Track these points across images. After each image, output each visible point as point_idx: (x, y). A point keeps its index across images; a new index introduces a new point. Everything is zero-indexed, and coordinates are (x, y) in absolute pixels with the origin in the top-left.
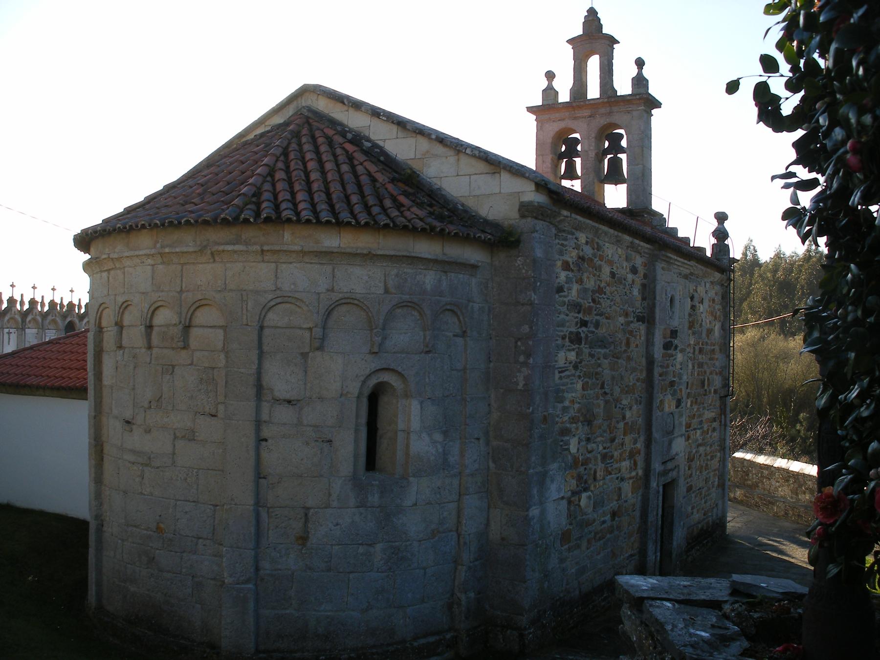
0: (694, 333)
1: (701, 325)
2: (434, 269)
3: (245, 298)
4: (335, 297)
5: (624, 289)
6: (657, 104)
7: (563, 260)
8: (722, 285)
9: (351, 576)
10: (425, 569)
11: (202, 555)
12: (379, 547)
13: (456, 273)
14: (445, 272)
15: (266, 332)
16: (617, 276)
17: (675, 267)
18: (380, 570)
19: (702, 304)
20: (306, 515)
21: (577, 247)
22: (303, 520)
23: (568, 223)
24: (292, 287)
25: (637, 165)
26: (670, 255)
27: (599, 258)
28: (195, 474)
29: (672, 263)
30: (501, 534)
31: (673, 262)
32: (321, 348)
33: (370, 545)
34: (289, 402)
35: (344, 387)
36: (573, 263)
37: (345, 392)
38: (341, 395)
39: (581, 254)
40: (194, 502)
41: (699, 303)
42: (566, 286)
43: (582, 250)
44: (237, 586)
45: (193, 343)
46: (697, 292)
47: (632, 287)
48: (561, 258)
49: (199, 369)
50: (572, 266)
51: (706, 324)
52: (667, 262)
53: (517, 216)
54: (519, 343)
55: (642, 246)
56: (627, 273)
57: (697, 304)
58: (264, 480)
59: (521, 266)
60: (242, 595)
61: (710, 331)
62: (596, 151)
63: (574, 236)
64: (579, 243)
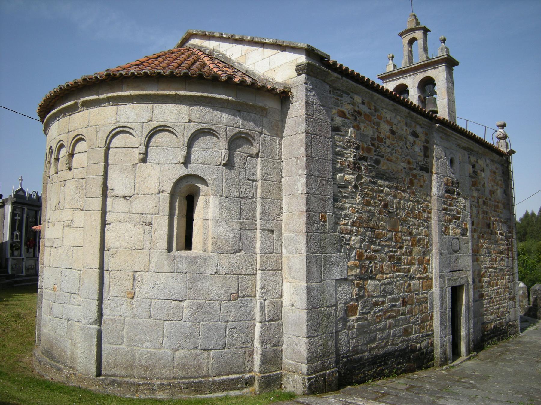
0: (477, 190)
1: (484, 186)
2: (229, 107)
3: (98, 130)
4: (154, 125)
5: (406, 144)
6: (429, 31)
7: (338, 109)
8: (502, 165)
9: (166, 323)
10: (226, 322)
11: (73, 305)
12: (185, 304)
13: (248, 112)
14: (239, 111)
15: (111, 151)
16: (396, 133)
17: (453, 139)
18: (187, 320)
19: (484, 172)
20: (134, 276)
21: (353, 104)
22: (132, 280)
23: (341, 84)
24: (126, 120)
25: (444, 99)
26: (446, 128)
27: (377, 117)
28: (71, 250)
29: (450, 136)
30: (290, 301)
31: (450, 134)
32: (144, 160)
33: (180, 301)
34: (124, 197)
35: (161, 187)
36: (349, 113)
37: (161, 190)
38: (159, 192)
39: (357, 109)
40: (70, 269)
41: (481, 171)
42: (343, 128)
43: (358, 107)
44: (88, 326)
45: (74, 164)
46: (477, 162)
47: (413, 145)
48: (337, 108)
49: (76, 181)
50: (347, 115)
51: (489, 185)
52: (445, 134)
53: (295, 74)
54: (299, 161)
55: (419, 119)
56: (408, 135)
57: (479, 171)
58: (107, 251)
59: (298, 108)
60: (90, 332)
61: (492, 192)
62: (419, 95)
63: (350, 96)
64: (355, 101)
